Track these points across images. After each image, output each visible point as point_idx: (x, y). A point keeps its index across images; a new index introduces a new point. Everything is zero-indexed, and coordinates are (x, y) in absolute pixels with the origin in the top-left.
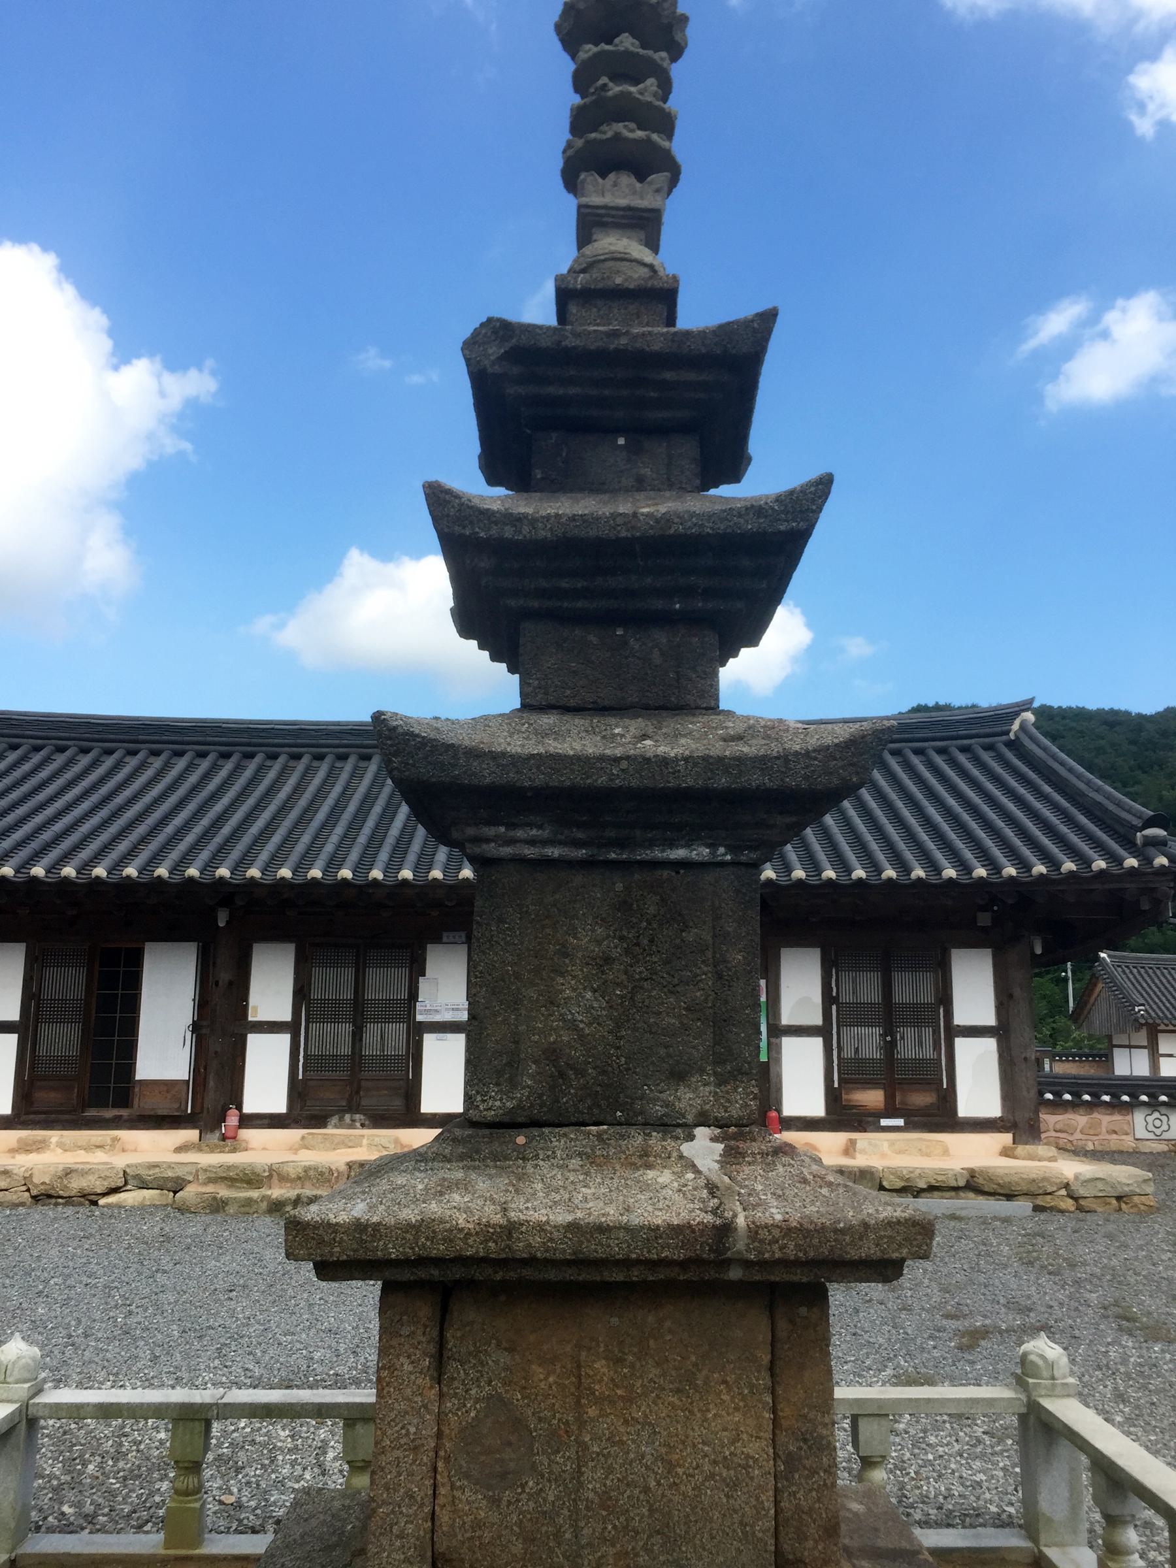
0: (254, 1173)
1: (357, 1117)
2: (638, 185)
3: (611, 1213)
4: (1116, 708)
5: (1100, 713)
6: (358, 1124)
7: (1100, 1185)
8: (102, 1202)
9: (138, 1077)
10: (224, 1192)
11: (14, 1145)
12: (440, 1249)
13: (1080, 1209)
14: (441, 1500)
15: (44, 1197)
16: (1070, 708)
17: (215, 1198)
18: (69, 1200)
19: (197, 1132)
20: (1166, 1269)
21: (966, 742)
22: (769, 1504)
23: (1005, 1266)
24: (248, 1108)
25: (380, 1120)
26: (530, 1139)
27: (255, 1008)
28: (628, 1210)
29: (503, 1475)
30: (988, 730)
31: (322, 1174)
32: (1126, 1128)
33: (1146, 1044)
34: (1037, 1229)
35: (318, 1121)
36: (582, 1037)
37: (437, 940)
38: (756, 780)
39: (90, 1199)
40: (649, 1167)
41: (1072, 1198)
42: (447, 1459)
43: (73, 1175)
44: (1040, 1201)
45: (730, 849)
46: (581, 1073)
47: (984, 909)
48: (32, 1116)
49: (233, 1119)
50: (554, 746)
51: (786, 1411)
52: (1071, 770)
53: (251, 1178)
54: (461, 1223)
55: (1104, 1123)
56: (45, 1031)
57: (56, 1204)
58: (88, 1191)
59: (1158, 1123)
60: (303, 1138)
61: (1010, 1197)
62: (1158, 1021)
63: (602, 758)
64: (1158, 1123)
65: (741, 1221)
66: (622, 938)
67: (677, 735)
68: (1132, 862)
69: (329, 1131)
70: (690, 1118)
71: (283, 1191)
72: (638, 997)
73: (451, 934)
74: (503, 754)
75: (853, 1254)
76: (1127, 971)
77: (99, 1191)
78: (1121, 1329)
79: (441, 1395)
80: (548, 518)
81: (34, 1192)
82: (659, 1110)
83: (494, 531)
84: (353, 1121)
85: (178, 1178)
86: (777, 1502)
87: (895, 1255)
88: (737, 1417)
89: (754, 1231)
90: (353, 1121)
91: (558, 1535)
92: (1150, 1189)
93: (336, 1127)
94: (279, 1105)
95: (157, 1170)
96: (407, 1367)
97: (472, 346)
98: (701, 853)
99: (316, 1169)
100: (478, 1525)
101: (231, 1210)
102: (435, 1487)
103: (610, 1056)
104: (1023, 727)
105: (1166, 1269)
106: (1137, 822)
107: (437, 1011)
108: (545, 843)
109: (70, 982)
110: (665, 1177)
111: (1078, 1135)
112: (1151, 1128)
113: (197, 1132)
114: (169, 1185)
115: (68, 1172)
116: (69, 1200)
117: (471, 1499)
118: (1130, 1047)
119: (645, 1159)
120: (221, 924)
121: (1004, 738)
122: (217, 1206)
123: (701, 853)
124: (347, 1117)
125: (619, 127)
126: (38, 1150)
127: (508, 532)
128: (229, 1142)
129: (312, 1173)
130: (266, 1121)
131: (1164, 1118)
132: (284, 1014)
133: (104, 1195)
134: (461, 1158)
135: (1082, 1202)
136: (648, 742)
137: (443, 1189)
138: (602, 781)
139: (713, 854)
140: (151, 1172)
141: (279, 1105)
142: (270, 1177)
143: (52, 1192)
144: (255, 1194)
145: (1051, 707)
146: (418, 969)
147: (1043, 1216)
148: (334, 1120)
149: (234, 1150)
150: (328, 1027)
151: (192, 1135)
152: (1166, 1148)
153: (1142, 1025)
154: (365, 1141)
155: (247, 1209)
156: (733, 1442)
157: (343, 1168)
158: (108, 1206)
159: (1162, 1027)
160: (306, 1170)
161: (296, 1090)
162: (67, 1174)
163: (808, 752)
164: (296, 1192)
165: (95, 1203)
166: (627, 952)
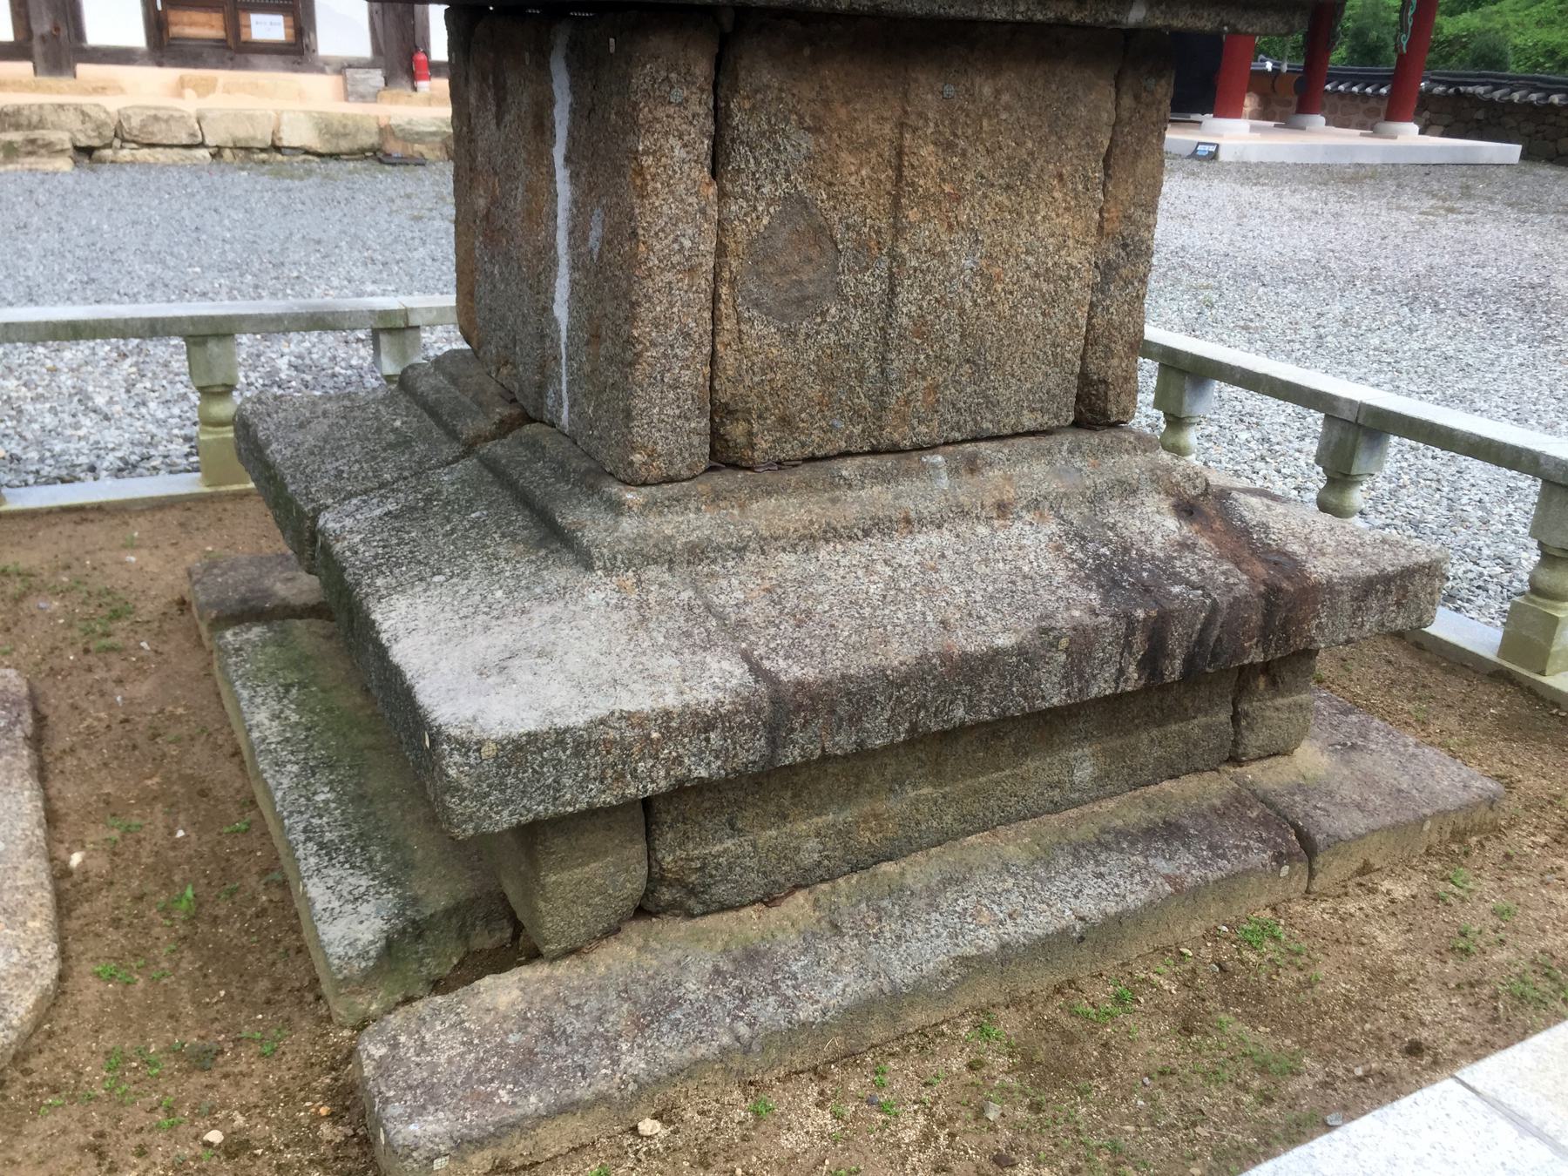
14: (725, 337)
22: (1083, 322)
29: (800, 302)
42: (732, 283)
79: (722, 195)
86: (1090, 318)
88: (1066, 219)
91: (861, 375)
96: (679, 153)
100: (771, 366)
102: (715, 319)
117: (761, 330)
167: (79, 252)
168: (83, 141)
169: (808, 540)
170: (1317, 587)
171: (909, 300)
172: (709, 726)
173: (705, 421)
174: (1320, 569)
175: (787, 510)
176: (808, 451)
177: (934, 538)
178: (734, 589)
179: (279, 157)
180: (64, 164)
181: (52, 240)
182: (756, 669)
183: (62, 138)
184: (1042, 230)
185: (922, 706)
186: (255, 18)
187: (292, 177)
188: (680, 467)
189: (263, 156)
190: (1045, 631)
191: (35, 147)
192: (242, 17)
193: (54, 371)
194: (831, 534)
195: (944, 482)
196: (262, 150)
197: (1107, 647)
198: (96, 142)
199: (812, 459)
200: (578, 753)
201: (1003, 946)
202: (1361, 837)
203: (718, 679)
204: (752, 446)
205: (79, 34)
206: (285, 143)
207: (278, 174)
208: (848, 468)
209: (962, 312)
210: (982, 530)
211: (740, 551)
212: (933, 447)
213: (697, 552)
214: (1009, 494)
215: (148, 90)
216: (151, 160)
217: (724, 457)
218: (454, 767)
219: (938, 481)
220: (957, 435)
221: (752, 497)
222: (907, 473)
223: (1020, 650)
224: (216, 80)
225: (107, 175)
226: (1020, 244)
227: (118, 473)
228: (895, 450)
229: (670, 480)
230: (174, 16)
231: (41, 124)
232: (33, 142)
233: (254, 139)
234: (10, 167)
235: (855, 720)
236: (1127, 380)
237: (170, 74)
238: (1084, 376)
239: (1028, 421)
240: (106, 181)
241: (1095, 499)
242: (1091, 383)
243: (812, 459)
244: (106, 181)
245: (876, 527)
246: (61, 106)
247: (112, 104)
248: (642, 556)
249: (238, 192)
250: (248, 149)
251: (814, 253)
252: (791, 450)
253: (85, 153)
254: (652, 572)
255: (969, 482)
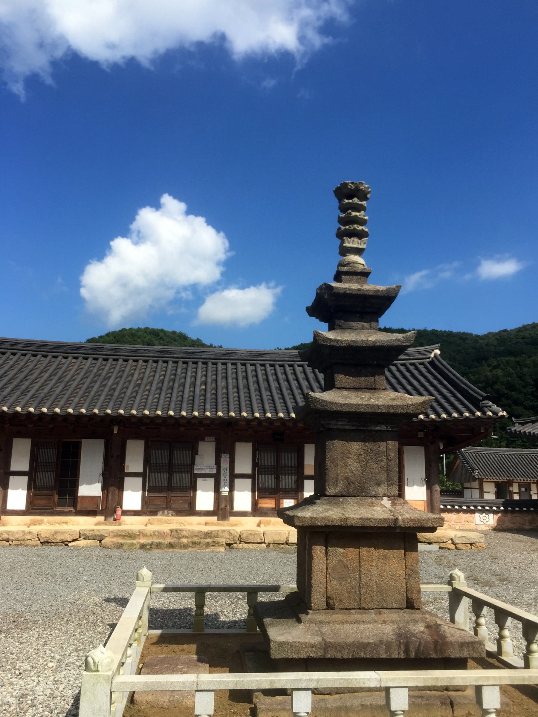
0: (132, 533)
1: (170, 512)
2: (359, 241)
3: (369, 516)
4: (466, 332)
5: (459, 333)
6: (170, 515)
7: (464, 539)
8: (70, 544)
9: (79, 495)
10: (121, 541)
11: (29, 522)
12: (330, 523)
13: (456, 548)
14: (328, 584)
15: (46, 543)
16: (445, 331)
17: (118, 543)
18: (56, 544)
19: (103, 517)
20: (489, 566)
21: (413, 361)
22: (405, 586)
23: (432, 566)
24: (125, 507)
25: (179, 513)
26: (343, 499)
27: (128, 466)
28: (373, 515)
29: (342, 578)
30: (421, 357)
31: (160, 534)
32: (472, 520)
33: (478, 487)
34: (441, 554)
35: (154, 513)
36: (354, 474)
37: (203, 440)
38: (400, 411)
39: (65, 543)
40: (374, 506)
41: (453, 544)
42: (329, 574)
43: (58, 534)
44: (441, 545)
45: (391, 427)
46: (354, 483)
47: (421, 431)
48: (34, 511)
49: (119, 512)
50: (349, 401)
51: (408, 564)
52: (454, 375)
53: (131, 535)
54: (335, 517)
55: (464, 518)
56: (39, 475)
57: (51, 546)
58: (64, 540)
59: (485, 518)
60: (149, 520)
61: (430, 544)
62: (484, 477)
63: (362, 405)
64: (485, 518)
65: (400, 518)
66: (364, 449)
67: (379, 398)
68: (479, 414)
69: (158, 517)
70: (381, 495)
71: (145, 540)
72: (368, 464)
73: (209, 437)
74: (339, 403)
75: (426, 525)
76: (471, 454)
77: (69, 540)
78: (474, 583)
79: (327, 559)
80: (345, 341)
81: (42, 541)
82: (374, 493)
83: (332, 343)
84: (168, 513)
85: (102, 535)
86: (406, 585)
87: (436, 526)
88: (397, 565)
89: (403, 520)
90: (168, 513)
91: (356, 592)
92: (482, 540)
93: (161, 515)
94: (138, 506)
95: (93, 532)
96: (319, 553)
97: (321, 288)
98: (383, 428)
99: (158, 532)
100: (337, 590)
101: (125, 547)
102: (326, 581)
103: (361, 479)
104: (435, 356)
105: (489, 566)
106: (480, 398)
107: (203, 469)
108: (345, 425)
109: (50, 455)
110: (379, 508)
111: (453, 523)
112: (482, 520)
113: (103, 517)
114: (98, 538)
115: (56, 532)
116: (56, 544)
117: (335, 583)
118: (471, 488)
119: (372, 505)
120: (115, 432)
121: (428, 360)
122: (120, 546)
123: (383, 428)
124: (166, 512)
125: (355, 226)
126: (39, 524)
127: (335, 344)
128: (118, 521)
129: (156, 533)
130: (133, 513)
131: (487, 516)
132: (140, 470)
133: (70, 542)
134: (327, 504)
135: (457, 546)
136: (372, 400)
137: (327, 510)
138: (362, 410)
139: (387, 428)
140: (90, 533)
141: (138, 506)
142: (139, 535)
143: (49, 541)
144: (135, 541)
145: (437, 331)
146: (195, 451)
147: (443, 551)
148: (161, 513)
149: (120, 524)
150: (158, 475)
151: (101, 518)
152: (488, 528)
153: (476, 479)
154: (175, 521)
155: (131, 547)
156: (396, 571)
157: (169, 532)
158: (73, 546)
159: (485, 480)
160: (154, 532)
161: (145, 501)
162: (56, 533)
163: (413, 405)
164: (152, 541)
165: (67, 545)
166: (365, 453)
167: (224, 576)
168: (229, 542)
169: (342, 623)
170: (447, 642)
171: (364, 579)
172: (313, 647)
173: (325, 599)
174: (450, 639)
175: (339, 617)
176: (346, 607)
177: (369, 626)
178: (326, 629)
179: (287, 546)
180: (222, 549)
181: (217, 572)
182: (323, 639)
183: (223, 541)
184: (392, 567)
185: (354, 651)
186: (285, 501)
187: (290, 554)
188: (320, 607)
189: (282, 546)
190: (380, 641)
191: (215, 544)
192: (281, 500)
193: (216, 606)
194: (347, 622)
195: (374, 615)
196: (283, 544)
197: (394, 646)
198: (232, 542)
199: (347, 609)
200: (291, 647)
201: (371, 705)
202: (466, 704)
203: (318, 639)
204: (334, 605)
205: (232, 507)
206: (290, 542)
207: (285, 553)
208: (353, 611)
209: (376, 582)
210: (380, 626)
211: (329, 623)
212: (373, 609)
213: (321, 622)
214: (386, 619)
215: (249, 524)
216: (248, 547)
217: (329, 607)
218: (272, 644)
219: (372, 615)
220: (378, 607)
221: (333, 614)
222: (365, 613)
223: (375, 643)
224: (270, 521)
225: (234, 553)
226: (388, 569)
227: (228, 628)
228: (364, 609)
229: (319, 610)
230: (260, 501)
231: (217, 537)
232: (214, 542)
233: (280, 540)
234: (207, 550)
235: (340, 651)
236: (418, 599)
237: (257, 519)
238: (407, 597)
239: (395, 606)
240: (234, 555)
241: (407, 622)
242: (409, 599)
243: (347, 609)
244: (234, 555)
245: (356, 622)
246: (224, 531)
247: (239, 529)
248: (311, 622)
249: (272, 558)
250: (278, 544)
251: (344, 569)
252: (342, 606)
253: (229, 545)
254: (312, 625)
255: (379, 616)
